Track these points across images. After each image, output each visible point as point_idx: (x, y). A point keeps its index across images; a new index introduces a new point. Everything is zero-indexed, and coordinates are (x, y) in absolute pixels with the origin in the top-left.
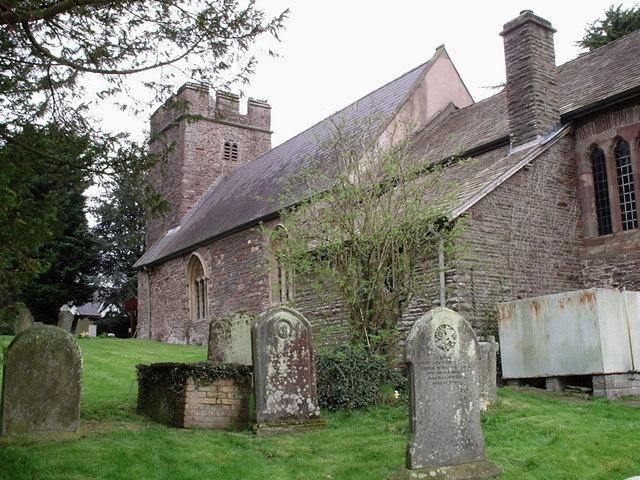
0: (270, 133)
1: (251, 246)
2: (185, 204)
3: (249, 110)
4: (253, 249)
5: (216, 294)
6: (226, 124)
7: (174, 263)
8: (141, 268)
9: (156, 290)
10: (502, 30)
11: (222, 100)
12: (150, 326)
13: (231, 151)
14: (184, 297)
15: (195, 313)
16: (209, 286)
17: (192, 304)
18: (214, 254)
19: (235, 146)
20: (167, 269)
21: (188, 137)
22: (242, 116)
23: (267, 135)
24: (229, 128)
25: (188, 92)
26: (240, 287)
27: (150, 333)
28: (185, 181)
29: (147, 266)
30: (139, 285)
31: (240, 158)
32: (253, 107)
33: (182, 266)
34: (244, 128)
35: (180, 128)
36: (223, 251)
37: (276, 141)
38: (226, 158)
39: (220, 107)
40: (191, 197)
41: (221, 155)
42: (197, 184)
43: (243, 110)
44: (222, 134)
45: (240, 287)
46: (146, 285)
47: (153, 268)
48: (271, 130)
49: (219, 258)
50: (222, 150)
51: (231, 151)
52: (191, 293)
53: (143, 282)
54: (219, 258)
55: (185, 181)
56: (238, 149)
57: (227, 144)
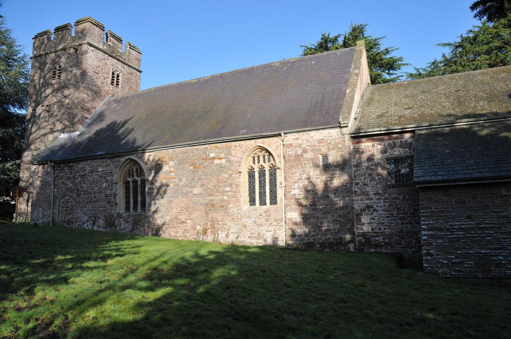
1: (214, 158)
24: (116, 61)
32: (131, 50)
45: (196, 191)
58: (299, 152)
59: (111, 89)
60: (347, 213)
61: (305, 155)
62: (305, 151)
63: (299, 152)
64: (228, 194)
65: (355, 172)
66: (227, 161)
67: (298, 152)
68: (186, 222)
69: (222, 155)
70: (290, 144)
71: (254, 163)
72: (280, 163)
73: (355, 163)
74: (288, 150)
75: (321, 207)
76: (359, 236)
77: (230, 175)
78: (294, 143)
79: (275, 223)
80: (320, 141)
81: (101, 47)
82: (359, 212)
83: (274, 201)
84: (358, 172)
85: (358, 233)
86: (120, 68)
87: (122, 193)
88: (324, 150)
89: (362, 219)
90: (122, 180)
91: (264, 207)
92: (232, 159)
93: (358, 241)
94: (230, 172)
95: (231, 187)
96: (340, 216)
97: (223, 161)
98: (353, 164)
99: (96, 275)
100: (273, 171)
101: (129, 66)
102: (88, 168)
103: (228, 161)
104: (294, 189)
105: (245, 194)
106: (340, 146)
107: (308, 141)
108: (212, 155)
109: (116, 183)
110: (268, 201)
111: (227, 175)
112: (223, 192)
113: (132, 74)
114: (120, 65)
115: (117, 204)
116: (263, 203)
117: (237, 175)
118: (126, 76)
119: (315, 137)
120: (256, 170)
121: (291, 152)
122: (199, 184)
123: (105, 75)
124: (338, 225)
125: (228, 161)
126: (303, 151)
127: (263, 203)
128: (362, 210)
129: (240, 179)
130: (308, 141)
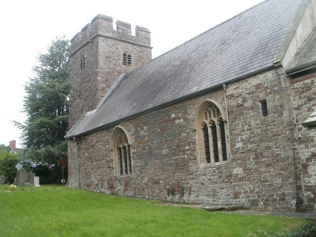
0: (151, 48)
1: (174, 119)
2: (99, 94)
3: (137, 34)
4: (177, 121)
5: (140, 157)
6: (124, 41)
7: (99, 134)
8: (71, 139)
9: (83, 153)
10: (47, 52)
11: (120, 26)
12: (80, 179)
13: (127, 59)
14: (109, 158)
15: (119, 169)
16: (132, 151)
17: (116, 164)
18: (136, 127)
19: (129, 56)
20: (93, 138)
21: (101, 49)
22: (132, 37)
23: (149, 49)
24: (126, 44)
25: (100, 20)
26: (165, 151)
27: (80, 183)
28: (99, 78)
29: (76, 137)
30: (69, 150)
31: (133, 64)
32: (139, 31)
33: (107, 136)
34: (136, 44)
35: (94, 44)
36: (145, 124)
37: (155, 54)
38: (124, 63)
39: (120, 31)
40: (103, 89)
41: (121, 61)
42: (107, 81)
43: (133, 34)
44: (122, 48)
45: (165, 151)
46: (75, 150)
47: (81, 138)
48: (151, 46)
49: (142, 129)
50: (122, 58)
51: (127, 59)
52: (115, 156)
53: (72, 148)
54: (142, 129)
55: (99, 78)
56: (132, 60)
57: (124, 55)
58: (240, 101)
59: (123, 68)
60: (289, 165)
61: (246, 105)
62: (244, 100)
63: (240, 101)
64: (187, 152)
65: (297, 115)
66: (184, 120)
67: (239, 102)
68: (159, 183)
69: (180, 115)
70: (231, 95)
71: (207, 119)
72: (224, 116)
73: (296, 106)
74: (230, 101)
75: (263, 160)
76: (307, 190)
77: (188, 134)
78: (235, 92)
79: (227, 180)
80: (258, 87)
81: (111, 36)
82: (305, 162)
83: (225, 158)
84: (300, 116)
85: (306, 186)
86: (130, 48)
87: (117, 159)
88: (262, 96)
89: (309, 171)
90: (116, 146)
91: (218, 164)
92: (189, 117)
93: (306, 196)
94: (187, 131)
95: (190, 146)
96: (282, 169)
97: (182, 120)
98: (294, 106)
99: (309, 214)
100: (222, 123)
101: (139, 45)
102: (95, 139)
103: (186, 119)
104: (238, 142)
105: (201, 151)
106: (276, 88)
107: (246, 89)
108: (173, 116)
109: (112, 150)
110: (221, 157)
111: (185, 134)
112: (184, 151)
113: (141, 51)
114: (130, 47)
115: (114, 169)
116: (217, 160)
117: (194, 133)
118: (137, 55)
119: (252, 84)
120: (209, 125)
121: (233, 103)
122: (165, 146)
123: (116, 58)
124: (280, 180)
125: (186, 119)
126: (243, 100)
127: (217, 160)
128: (309, 160)
129: (195, 136)
130: (246, 89)
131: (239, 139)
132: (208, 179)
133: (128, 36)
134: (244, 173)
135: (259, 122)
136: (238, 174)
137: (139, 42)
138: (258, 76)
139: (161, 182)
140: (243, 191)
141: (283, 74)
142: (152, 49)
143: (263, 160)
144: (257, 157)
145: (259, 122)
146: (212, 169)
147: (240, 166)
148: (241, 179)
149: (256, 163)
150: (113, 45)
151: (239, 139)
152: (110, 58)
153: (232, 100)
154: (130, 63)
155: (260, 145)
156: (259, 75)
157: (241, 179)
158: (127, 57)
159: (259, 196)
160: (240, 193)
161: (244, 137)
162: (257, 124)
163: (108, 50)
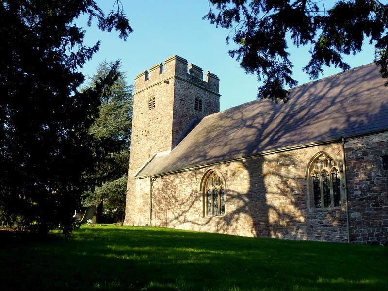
19: (201, 101)
23: (217, 97)
34: (207, 91)
39: (193, 75)
41: (193, 106)
48: (219, 93)
57: (196, 100)
67: (359, 155)
68: (259, 224)
75: (383, 207)
81: (185, 78)
86: (202, 94)
101: (209, 91)
104: (357, 190)
116: (327, 203)
123: (189, 101)
130: (367, 144)
131: (358, 187)
132: (319, 222)
133: (200, 81)
134: (363, 217)
135: (380, 174)
136: (355, 219)
137: (208, 88)
138: (380, 134)
139: (261, 223)
140: (361, 234)
141: (343, 146)
142: (220, 97)
143: (383, 207)
144: (377, 204)
145: (380, 174)
146: (324, 213)
147: (358, 212)
148: (359, 223)
149: (375, 210)
150: (187, 89)
151: (358, 187)
152: (184, 101)
153: (351, 153)
154: (201, 109)
155: (380, 194)
156: (381, 134)
157: (359, 223)
158: (199, 102)
159: (379, 239)
160: (358, 235)
161: (363, 186)
162: (378, 176)
163: (183, 92)
